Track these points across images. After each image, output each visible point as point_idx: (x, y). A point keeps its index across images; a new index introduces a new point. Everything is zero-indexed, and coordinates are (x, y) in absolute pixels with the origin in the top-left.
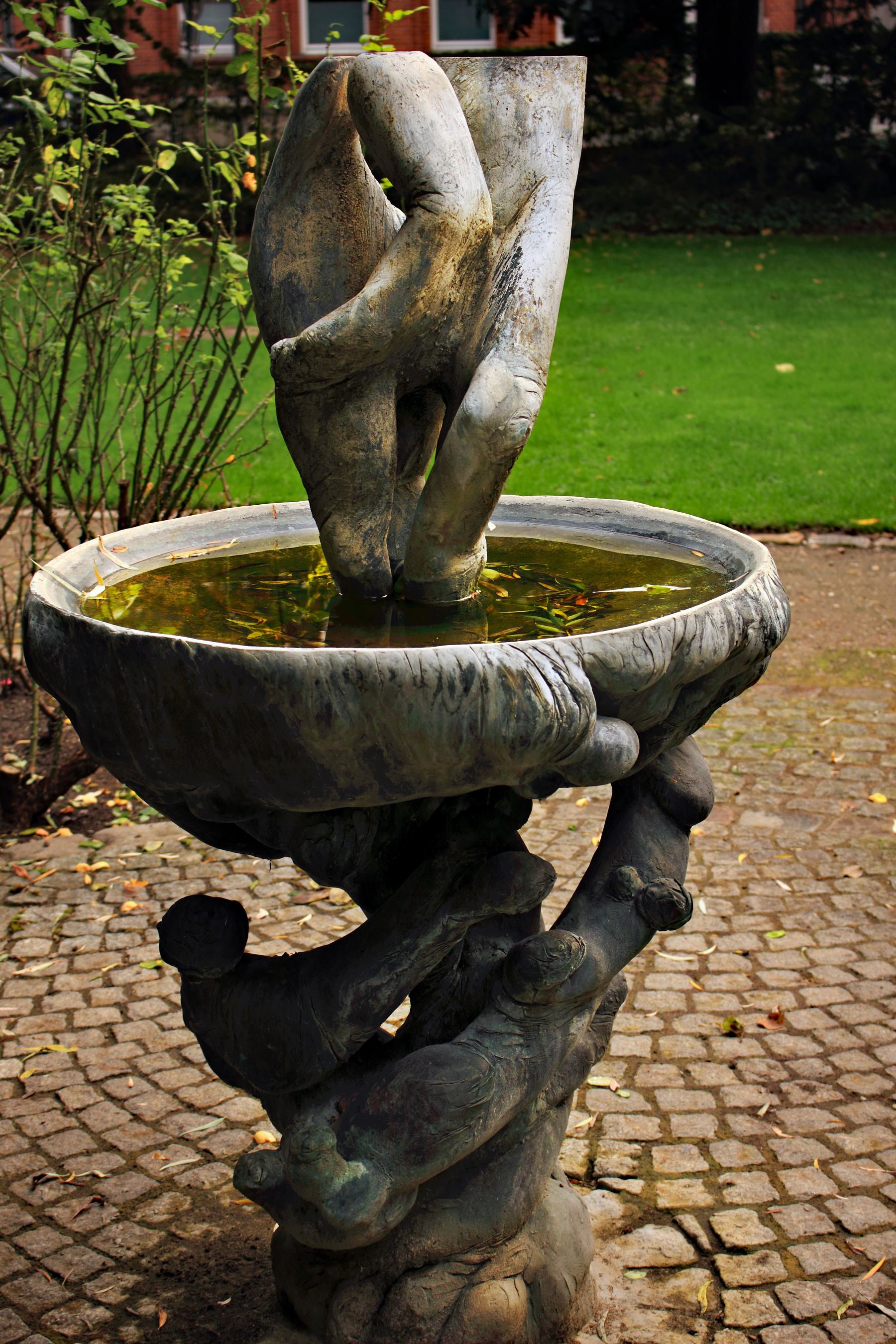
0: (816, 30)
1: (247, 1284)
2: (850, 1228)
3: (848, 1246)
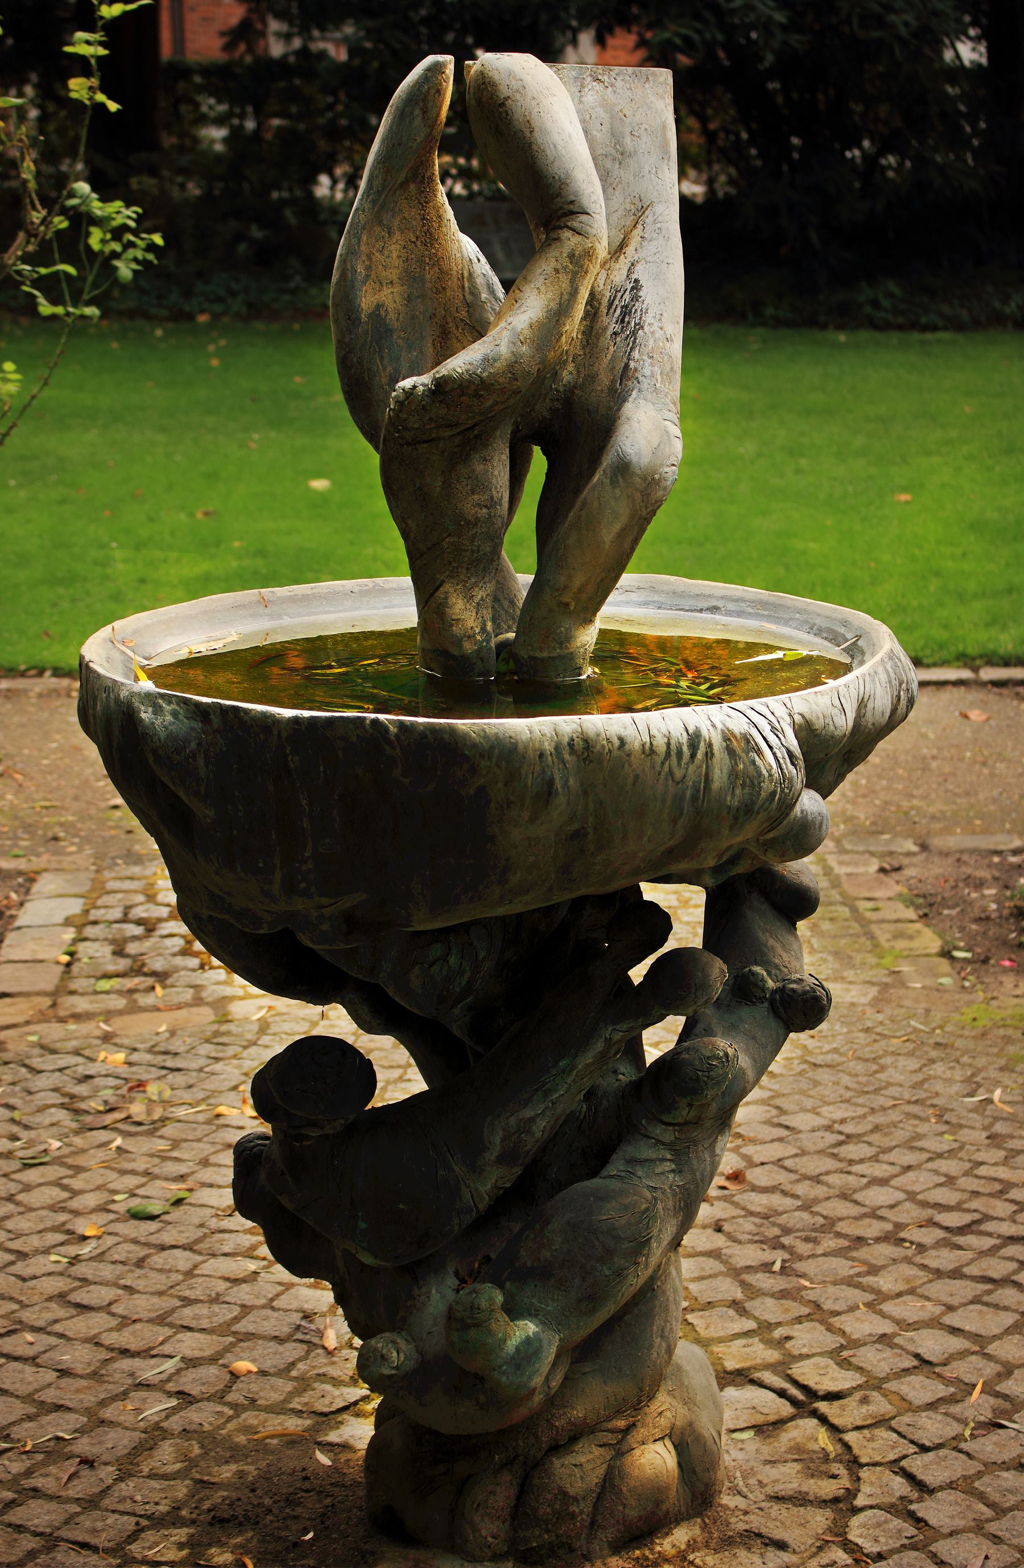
0: (248, 59)
1: (323, 1514)
2: (931, 1359)
3: (939, 1376)
